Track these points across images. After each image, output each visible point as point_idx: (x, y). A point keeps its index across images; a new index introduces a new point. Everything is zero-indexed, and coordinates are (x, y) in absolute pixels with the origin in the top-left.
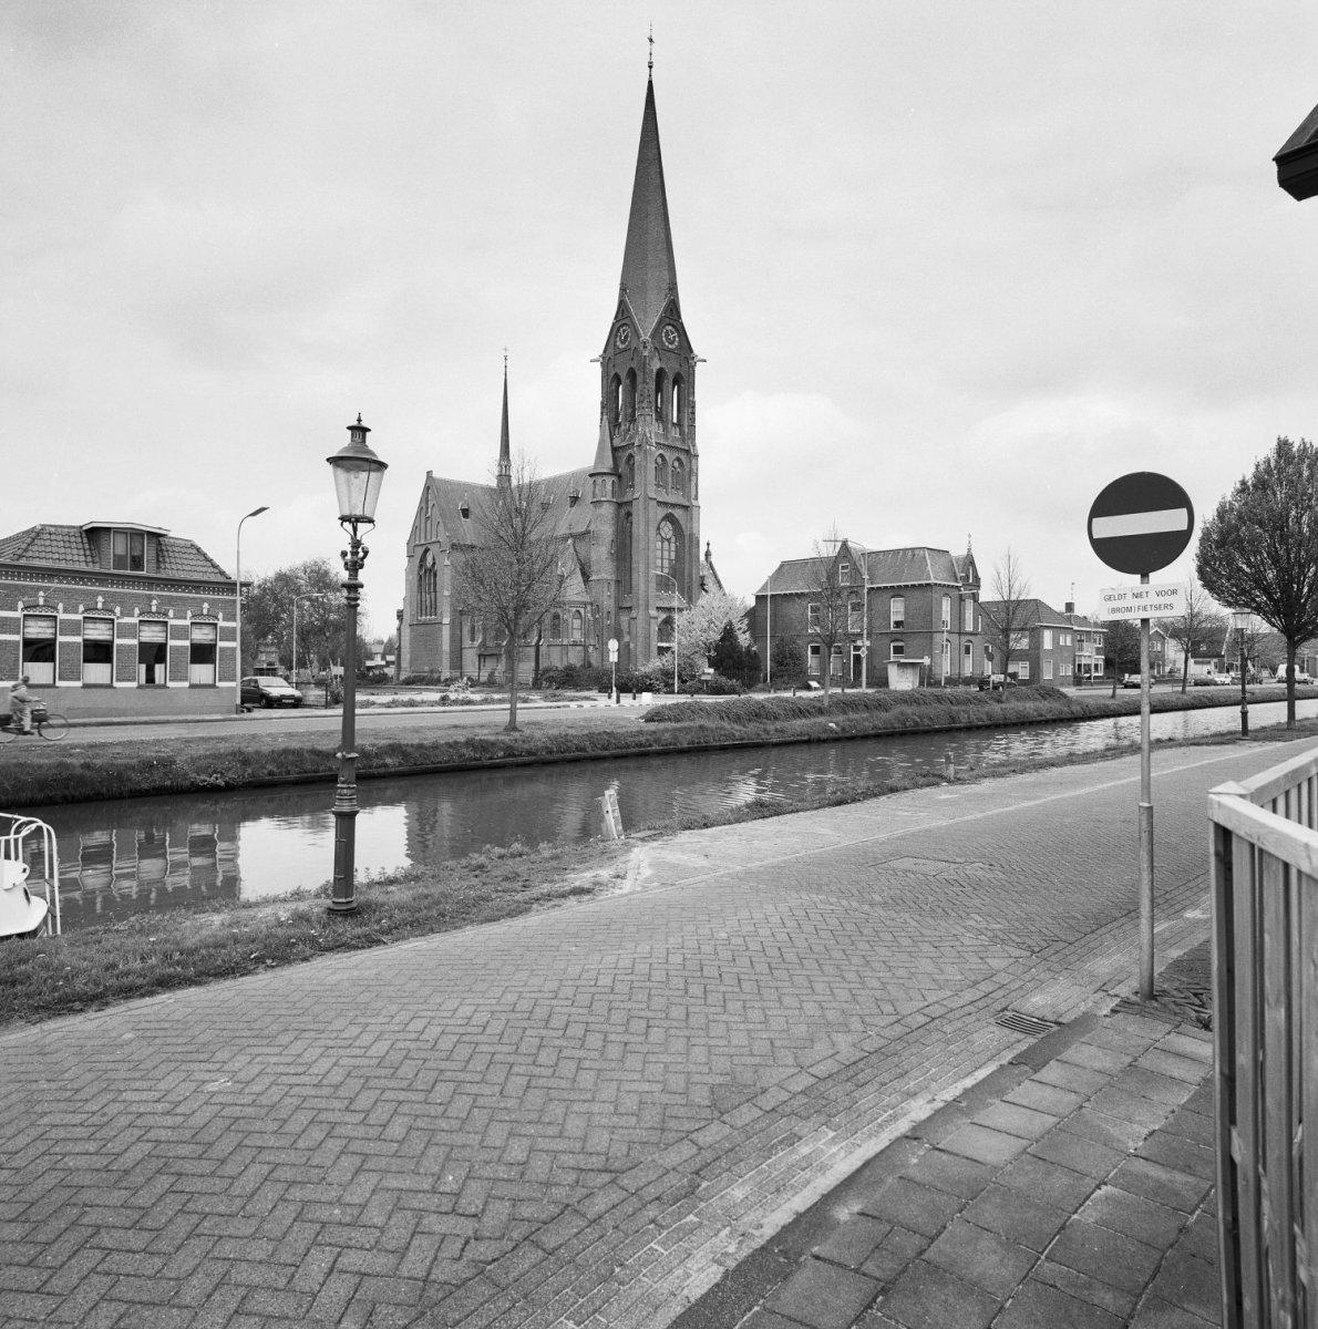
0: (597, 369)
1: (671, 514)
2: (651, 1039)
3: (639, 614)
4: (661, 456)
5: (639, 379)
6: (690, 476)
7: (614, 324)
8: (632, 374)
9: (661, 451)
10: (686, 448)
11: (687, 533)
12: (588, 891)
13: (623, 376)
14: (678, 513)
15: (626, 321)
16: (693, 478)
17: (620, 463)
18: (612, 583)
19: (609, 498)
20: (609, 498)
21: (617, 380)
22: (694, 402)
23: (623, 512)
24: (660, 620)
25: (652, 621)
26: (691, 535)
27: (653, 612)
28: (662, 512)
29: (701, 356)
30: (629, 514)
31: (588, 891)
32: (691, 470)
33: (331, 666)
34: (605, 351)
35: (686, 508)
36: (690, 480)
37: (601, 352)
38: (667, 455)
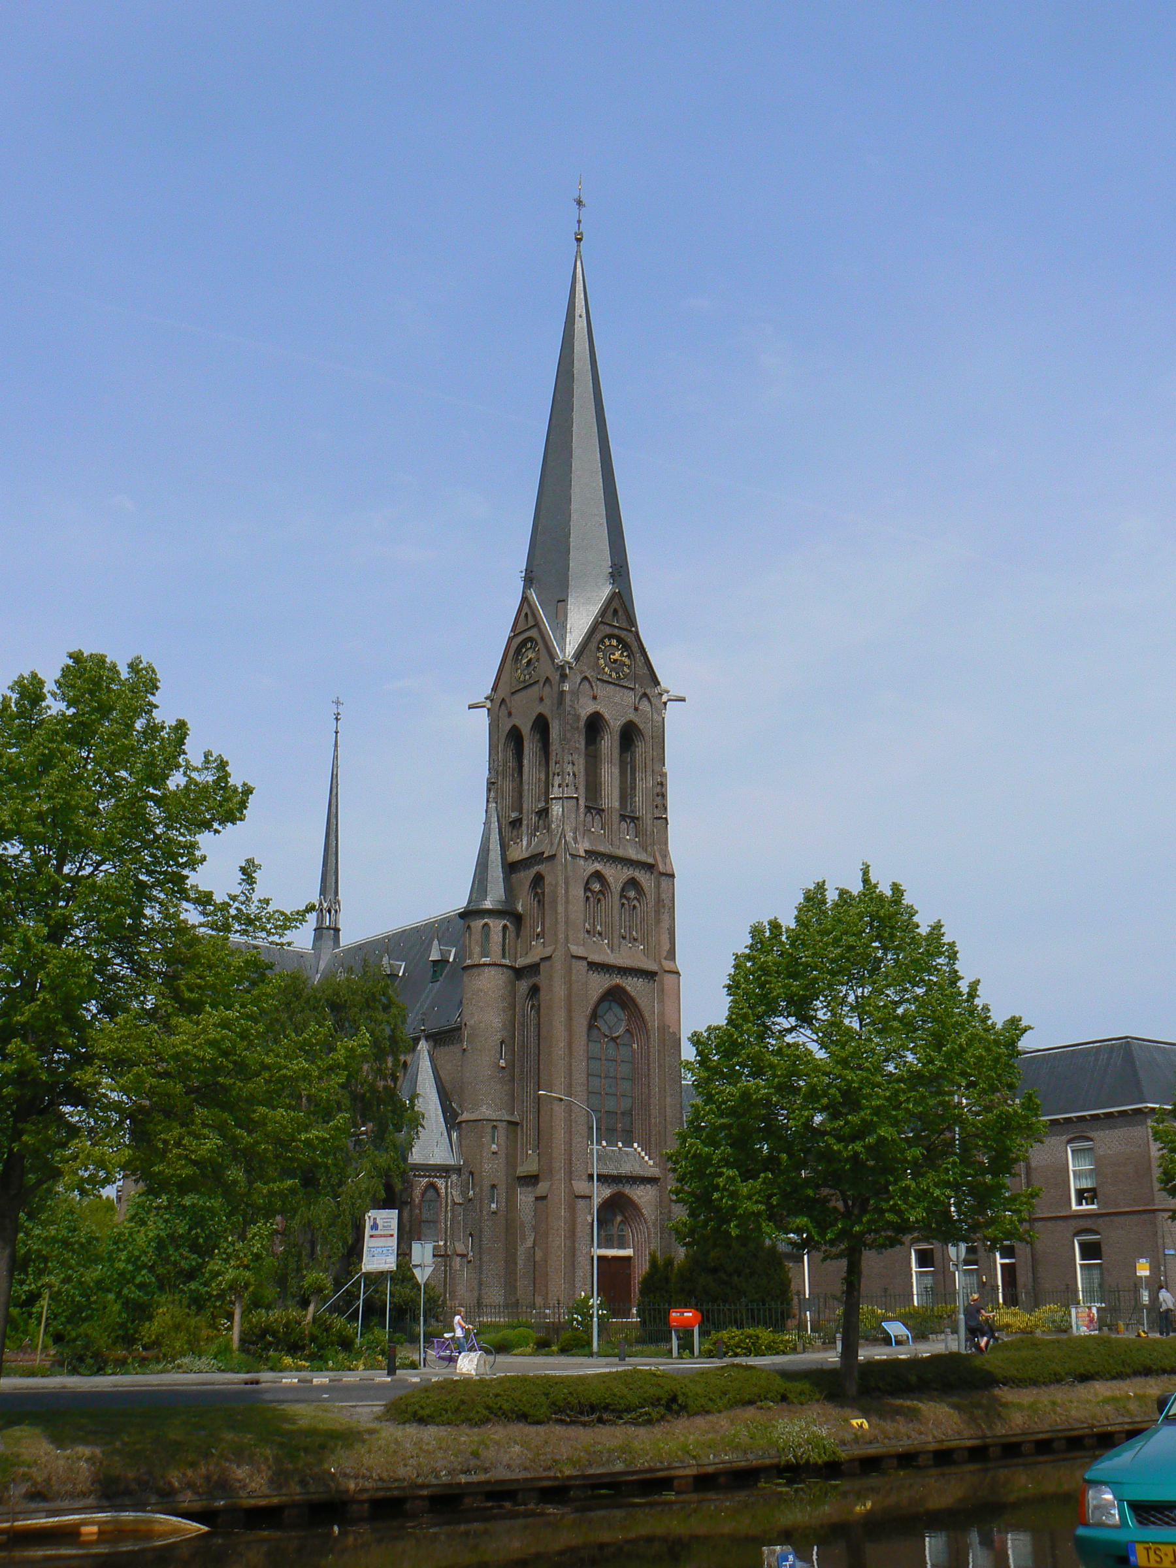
0: (482, 718)
1: (618, 986)
2: (673, 1205)
3: (555, 1187)
4: (598, 875)
5: (554, 733)
6: (657, 912)
7: (510, 639)
8: (541, 726)
9: (598, 866)
10: (650, 861)
11: (654, 1024)
12: (513, 693)
13: (526, 730)
14: (633, 986)
15: (533, 633)
16: (665, 917)
17: (519, 878)
18: (502, 1127)
19: (495, 956)
20: (495, 956)
21: (515, 736)
22: (664, 775)
23: (523, 986)
24: (596, 1202)
25: (581, 1203)
26: (663, 1028)
27: (581, 1186)
28: (599, 984)
29: (674, 693)
30: (534, 990)
31: (513, 693)
32: (659, 901)
33: (215, 1477)
34: (494, 689)
35: (650, 975)
36: (658, 921)
37: (488, 691)
38: (609, 871)
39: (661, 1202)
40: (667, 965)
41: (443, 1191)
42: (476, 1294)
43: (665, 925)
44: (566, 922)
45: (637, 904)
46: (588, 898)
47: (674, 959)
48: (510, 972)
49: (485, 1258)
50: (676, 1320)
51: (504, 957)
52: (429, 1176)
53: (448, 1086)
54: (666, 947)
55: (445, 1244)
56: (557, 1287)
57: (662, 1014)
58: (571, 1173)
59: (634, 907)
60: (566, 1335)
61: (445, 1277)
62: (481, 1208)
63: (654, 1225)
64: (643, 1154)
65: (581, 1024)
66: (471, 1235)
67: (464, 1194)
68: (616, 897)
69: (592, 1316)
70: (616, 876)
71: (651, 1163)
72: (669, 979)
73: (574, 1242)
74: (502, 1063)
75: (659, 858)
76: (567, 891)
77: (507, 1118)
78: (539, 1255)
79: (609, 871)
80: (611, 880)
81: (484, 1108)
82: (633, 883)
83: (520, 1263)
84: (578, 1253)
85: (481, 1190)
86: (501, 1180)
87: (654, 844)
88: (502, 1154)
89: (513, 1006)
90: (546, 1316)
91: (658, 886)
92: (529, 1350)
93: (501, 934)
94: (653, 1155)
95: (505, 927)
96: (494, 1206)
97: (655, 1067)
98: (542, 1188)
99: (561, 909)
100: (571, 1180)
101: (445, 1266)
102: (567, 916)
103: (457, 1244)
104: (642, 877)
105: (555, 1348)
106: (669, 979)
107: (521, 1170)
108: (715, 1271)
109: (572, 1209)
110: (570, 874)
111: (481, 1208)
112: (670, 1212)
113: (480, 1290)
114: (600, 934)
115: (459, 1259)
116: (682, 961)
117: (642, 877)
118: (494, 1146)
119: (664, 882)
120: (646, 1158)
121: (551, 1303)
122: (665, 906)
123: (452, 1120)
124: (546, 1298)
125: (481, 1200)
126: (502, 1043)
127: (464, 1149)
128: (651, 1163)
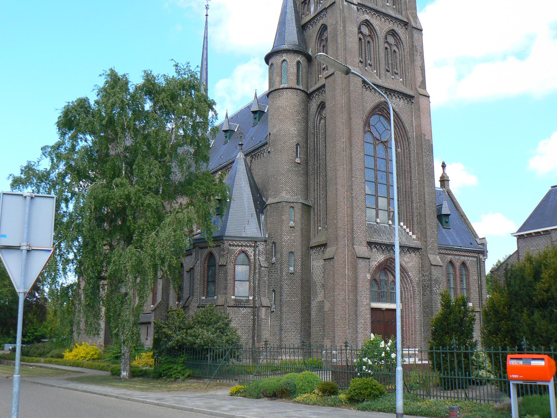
3: (340, 251)
9: (367, 17)
16: (418, 58)
23: (314, 105)
24: (374, 264)
25: (362, 264)
28: (372, 99)
35: (409, 98)
36: (413, 61)
38: (376, 22)
39: (422, 267)
40: (421, 91)
41: (252, 257)
42: (278, 337)
43: (418, 63)
44: (345, 49)
45: (397, 50)
46: (360, 39)
47: (425, 88)
48: (303, 94)
49: (285, 309)
50: (517, 369)
51: (298, 83)
52: (242, 246)
53: (260, 186)
54: (420, 79)
55: (254, 299)
56: (341, 333)
57: (419, 126)
58: (353, 238)
59: (395, 51)
60: (356, 382)
61: (254, 324)
62: (281, 269)
63: (418, 284)
64: (408, 230)
65: (358, 123)
66: (274, 291)
67: (267, 259)
68: (382, 40)
69: (395, 365)
70: (381, 26)
71: (414, 237)
72: (422, 100)
73: (356, 295)
74: (298, 160)
75: (411, 19)
76: (344, 27)
77: (301, 201)
78: (327, 306)
79: (376, 22)
80: (377, 28)
81: (284, 194)
82: (393, 33)
83: (313, 314)
84: (359, 303)
85: (281, 255)
86: (298, 248)
87: (406, 9)
88: (298, 228)
89: (306, 120)
90: (333, 356)
91: (412, 37)
92: (313, 397)
93: (295, 68)
94: (416, 231)
95: (298, 62)
96: (292, 269)
97: (414, 165)
98: (329, 252)
99: (340, 40)
100: (353, 244)
101: (254, 315)
102: (345, 45)
103: (262, 298)
104: (400, 30)
105: (342, 396)
106: (422, 100)
107: (313, 243)
108: (543, 305)
109: (355, 269)
110: (347, 15)
111: (281, 269)
112: (430, 274)
113: (281, 334)
114: (370, 65)
115: (264, 309)
116: (430, 89)
117: (400, 30)
118: (292, 222)
119: (416, 34)
120: (411, 233)
121: (339, 345)
122: (416, 52)
123: (260, 206)
124: (333, 341)
125: (281, 264)
126: (298, 144)
127: (269, 226)
128: (414, 237)
